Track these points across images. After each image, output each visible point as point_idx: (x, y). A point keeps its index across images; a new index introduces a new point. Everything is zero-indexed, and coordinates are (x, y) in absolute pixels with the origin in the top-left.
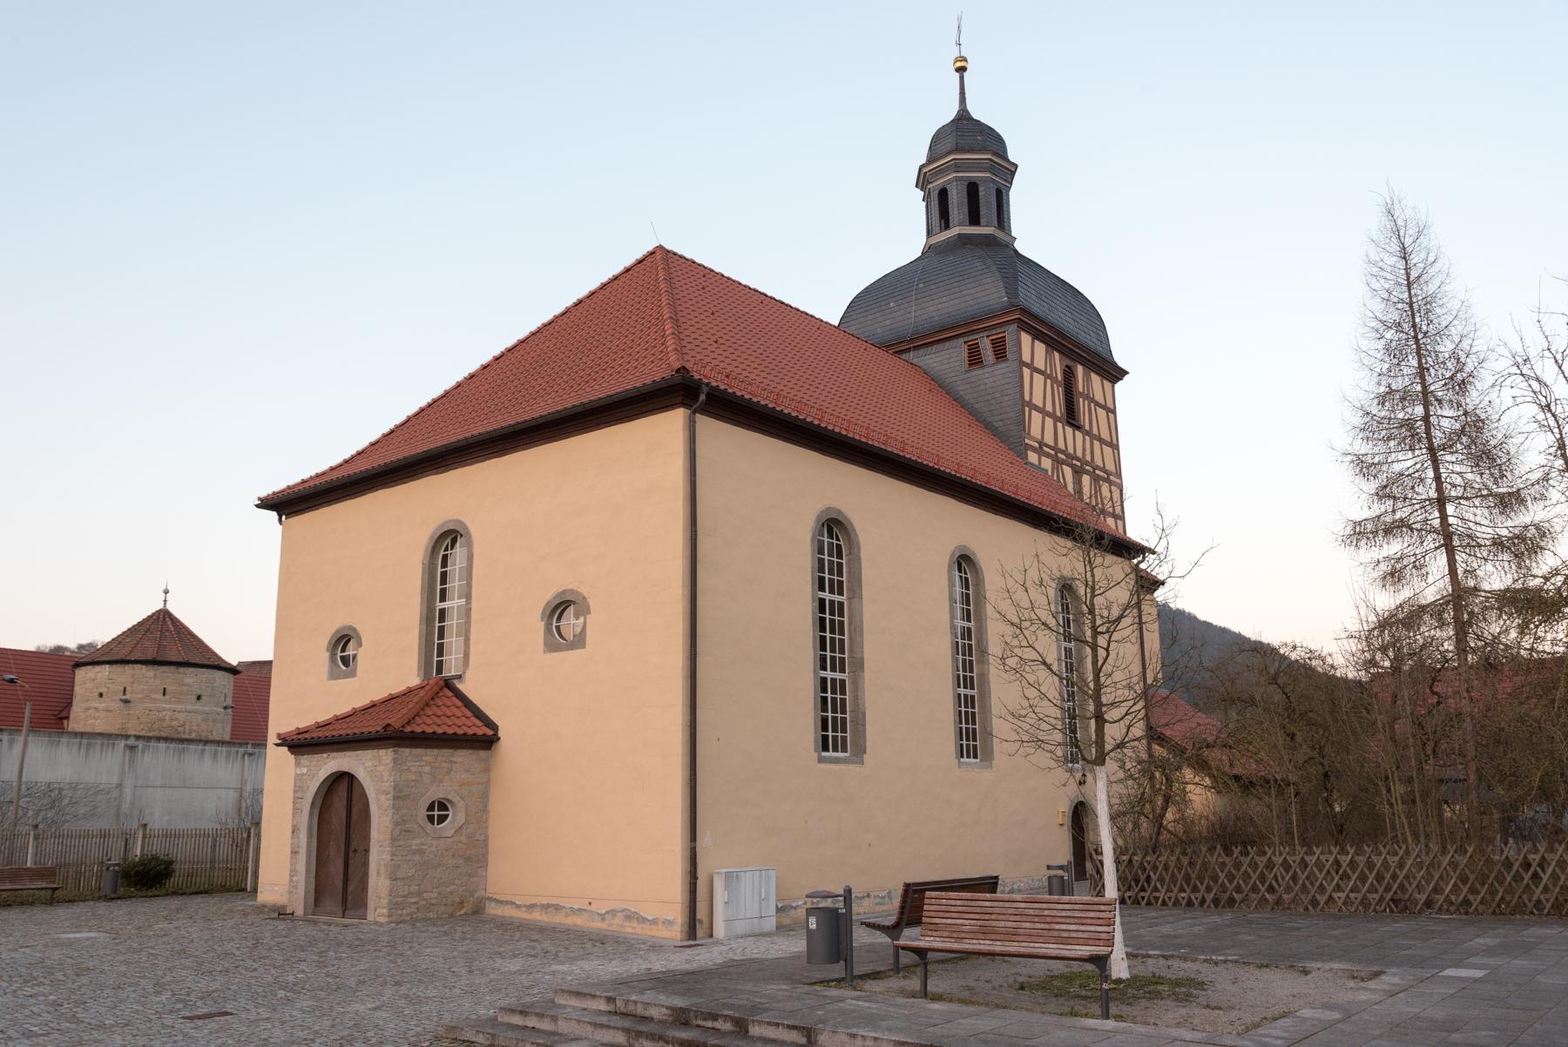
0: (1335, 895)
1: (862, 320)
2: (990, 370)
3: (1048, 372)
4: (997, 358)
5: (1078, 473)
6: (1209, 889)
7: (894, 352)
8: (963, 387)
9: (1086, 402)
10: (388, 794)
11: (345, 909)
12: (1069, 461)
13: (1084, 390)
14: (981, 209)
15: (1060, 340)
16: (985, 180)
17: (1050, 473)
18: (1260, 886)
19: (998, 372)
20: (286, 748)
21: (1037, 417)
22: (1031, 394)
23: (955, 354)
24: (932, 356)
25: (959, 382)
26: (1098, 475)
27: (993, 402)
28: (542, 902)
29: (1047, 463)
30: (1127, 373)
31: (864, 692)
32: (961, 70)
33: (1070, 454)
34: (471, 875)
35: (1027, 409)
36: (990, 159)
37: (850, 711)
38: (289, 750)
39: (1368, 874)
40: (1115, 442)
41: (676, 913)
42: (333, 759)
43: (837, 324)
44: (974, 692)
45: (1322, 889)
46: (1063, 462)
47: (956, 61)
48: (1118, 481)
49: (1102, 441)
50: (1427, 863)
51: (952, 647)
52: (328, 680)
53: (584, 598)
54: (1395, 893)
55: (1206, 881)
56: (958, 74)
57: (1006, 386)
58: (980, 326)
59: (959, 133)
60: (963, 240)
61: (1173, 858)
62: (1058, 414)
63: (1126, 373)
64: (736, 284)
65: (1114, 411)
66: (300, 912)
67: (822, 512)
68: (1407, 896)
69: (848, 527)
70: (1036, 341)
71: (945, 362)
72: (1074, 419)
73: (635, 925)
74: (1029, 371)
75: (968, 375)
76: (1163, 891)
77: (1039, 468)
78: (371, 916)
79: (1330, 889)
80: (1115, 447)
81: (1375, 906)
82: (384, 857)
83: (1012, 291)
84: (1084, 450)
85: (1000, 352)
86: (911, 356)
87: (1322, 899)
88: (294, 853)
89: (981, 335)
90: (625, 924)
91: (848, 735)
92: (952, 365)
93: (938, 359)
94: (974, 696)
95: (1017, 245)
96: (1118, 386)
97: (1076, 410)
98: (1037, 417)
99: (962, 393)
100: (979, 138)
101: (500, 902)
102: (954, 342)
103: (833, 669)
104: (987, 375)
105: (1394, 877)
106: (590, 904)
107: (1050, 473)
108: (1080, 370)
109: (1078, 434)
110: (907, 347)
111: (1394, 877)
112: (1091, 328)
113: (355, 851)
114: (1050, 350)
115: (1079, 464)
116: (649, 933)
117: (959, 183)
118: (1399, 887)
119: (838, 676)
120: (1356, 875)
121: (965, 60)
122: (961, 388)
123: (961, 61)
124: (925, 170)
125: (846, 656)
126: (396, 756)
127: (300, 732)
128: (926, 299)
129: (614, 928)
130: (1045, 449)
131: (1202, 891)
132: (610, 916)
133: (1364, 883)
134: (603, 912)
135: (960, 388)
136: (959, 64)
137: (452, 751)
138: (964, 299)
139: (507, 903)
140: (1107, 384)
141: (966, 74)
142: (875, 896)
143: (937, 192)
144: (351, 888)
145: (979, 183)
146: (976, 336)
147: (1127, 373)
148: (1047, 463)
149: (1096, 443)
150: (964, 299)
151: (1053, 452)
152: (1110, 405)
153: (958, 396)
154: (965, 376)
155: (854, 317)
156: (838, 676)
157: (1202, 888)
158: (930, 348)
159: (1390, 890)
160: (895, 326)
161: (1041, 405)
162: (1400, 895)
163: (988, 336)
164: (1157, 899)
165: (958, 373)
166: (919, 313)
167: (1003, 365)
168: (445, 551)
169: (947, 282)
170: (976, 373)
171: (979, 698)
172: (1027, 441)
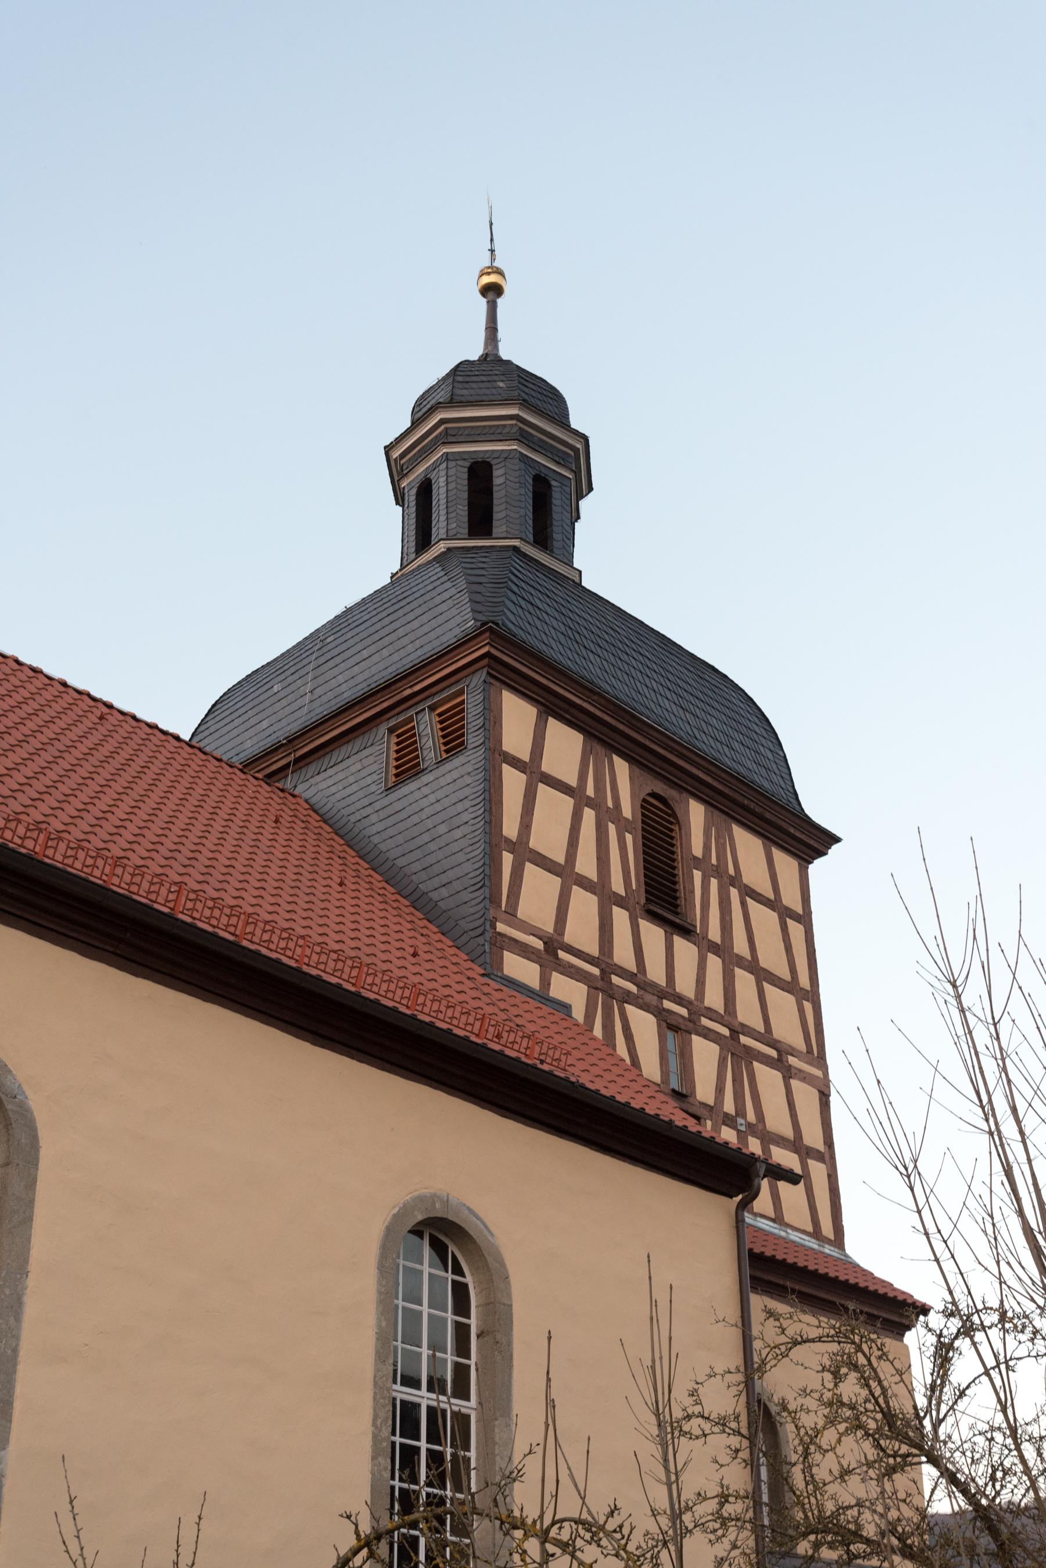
3: (590, 791)
4: (447, 751)
7: (269, 776)
8: (380, 827)
9: (714, 882)
12: (652, 999)
13: (707, 848)
14: (495, 509)
15: (621, 727)
16: (507, 456)
17: (579, 1014)
19: (449, 778)
23: (371, 759)
25: (374, 818)
27: (433, 846)
30: (837, 840)
33: (654, 985)
35: (507, 858)
40: (804, 981)
46: (627, 998)
48: (818, 1073)
49: (763, 976)
57: (460, 807)
58: (417, 688)
59: (460, 379)
62: (618, 886)
65: (805, 919)
70: (551, 721)
71: (352, 779)
72: (677, 914)
77: (542, 996)
92: (363, 783)
93: (341, 776)
95: (585, 583)
96: (817, 868)
97: (681, 894)
99: (376, 840)
100: (501, 384)
107: (579, 1014)
108: (696, 813)
109: (685, 950)
114: (600, 749)
117: (452, 464)
121: (500, 272)
123: (489, 274)
124: (395, 454)
130: (562, 954)
135: (374, 830)
136: (486, 280)
141: (500, 301)
143: (414, 491)
145: (493, 462)
147: (837, 840)
149: (744, 981)
151: (596, 971)
152: (791, 899)
154: (386, 801)
163: (432, 708)
165: (373, 798)
166: (319, 691)
167: (457, 761)
172: (501, 927)
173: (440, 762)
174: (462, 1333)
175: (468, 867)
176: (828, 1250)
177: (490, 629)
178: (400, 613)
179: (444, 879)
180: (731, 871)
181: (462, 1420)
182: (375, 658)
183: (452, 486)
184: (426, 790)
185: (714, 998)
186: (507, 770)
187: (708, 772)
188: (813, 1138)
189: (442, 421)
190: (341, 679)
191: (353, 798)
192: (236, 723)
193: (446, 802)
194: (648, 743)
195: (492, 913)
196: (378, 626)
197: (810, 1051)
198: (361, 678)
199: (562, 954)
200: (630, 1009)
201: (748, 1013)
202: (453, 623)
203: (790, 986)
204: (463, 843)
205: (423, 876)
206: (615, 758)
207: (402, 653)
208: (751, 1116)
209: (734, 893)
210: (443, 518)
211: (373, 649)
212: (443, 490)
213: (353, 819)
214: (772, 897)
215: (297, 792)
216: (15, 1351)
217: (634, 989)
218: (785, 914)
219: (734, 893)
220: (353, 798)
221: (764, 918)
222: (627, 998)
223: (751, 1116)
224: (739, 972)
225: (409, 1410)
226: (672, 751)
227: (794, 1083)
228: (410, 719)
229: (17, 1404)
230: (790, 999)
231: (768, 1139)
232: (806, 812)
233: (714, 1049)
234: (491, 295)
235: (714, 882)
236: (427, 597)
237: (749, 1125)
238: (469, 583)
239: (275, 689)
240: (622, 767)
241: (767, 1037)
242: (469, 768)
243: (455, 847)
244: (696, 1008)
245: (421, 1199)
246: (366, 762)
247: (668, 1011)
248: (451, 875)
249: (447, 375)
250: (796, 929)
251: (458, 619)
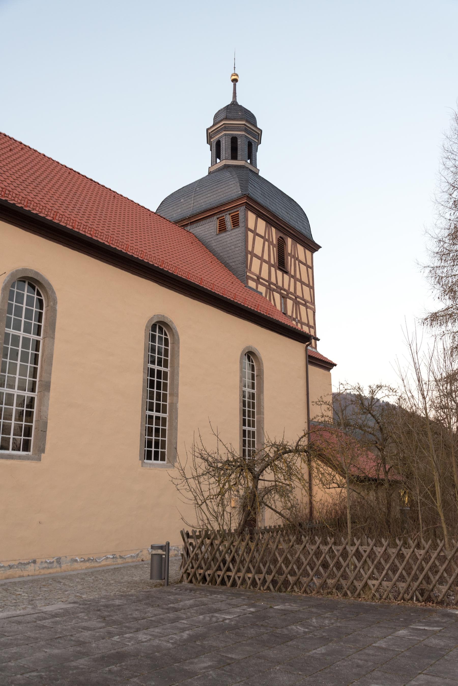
0: (370, 582)
1: (167, 210)
3: (267, 237)
4: (234, 226)
5: (284, 297)
6: (269, 572)
8: (215, 244)
9: (293, 259)
12: (279, 290)
13: (291, 251)
14: (238, 151)
15: (274, 220)
16: (242, 136)
17: (264, 295)
18: (310, 572)
19: (234, 234)
21: (255, 260)
22: (253, 247)
23: (212, 225)
25: (213, 241)
26: (299, 302)
27: (230, 251)
29: (262, 289)
30: (320, 247)
31: (48, 407)
33: (279, 287)
35: (249, 256)
36: (244, 124)
37: (36, 421)
39: (398, 565)
40: (311, 284)
43: (155, 212)
44: (255, 429)
45: (358, 577)
46: (274, 290)
47: (232, 75)
48: (313, 307)
49: (302, 283)
50: (449, 558)
51: (144, 382)
54: (421, 583)
55: (268, 564)
56: (233, 83)
57: (238, 242)
58: (225, 208)
60: (226, 167)
61: (244, 544)
62: (272, 262)
63: (320, 247)
64: (56, 164)
65: (312, 268)
67: (17, 271)
68: (431, 587)
69: (43, 282)
70: (259, 218)
71: (206, 230)
74: (252, 234)
75: (218, 237)
76: (234, 571)
77: (256, 291)
79: (366, 577)
80: (312, 287)
81: (403, 595)
83: (244, 187)
84: (289, 286)
85: (236, 224)
86: (188, 228)
87: (359, 585)
91: (32, 438)
92: (210, 232)
93: (203, 229)
94: (254, 432)
95: (259, 174)
96: (315, 254)
98: (255, 260)
99: (214, 247)
103: (249, 426)
105: (421, 569)
107: (264, 295)
108: (289, 241)
109: (286, 277)
110: (187, 223)
111: (421, 569)
112: (299, 219)
114: (269, 225)
115: (285, 293)
117: (226, 137)
118: (424, 578)
119: (251, 429)
120: (388, 565)
121: (237, 75)
122: (214, 244)
124: (210, 131)
125: (37, 380)
128: (199, 196)
130: (261, 280)
131: (264, 573)
133: (394, 572)
135: (213, 245)
136: (233, 77)
138: (219, 194)
141: (237, 84)
142: (42, 562)
143: (215, 143)
146: (223, 214)
147: (320, 247)
148: (262, 289)
149: (298, 284)
150: (219, 194)
151: (267, 284)
152: (309, 263)
153: (212, 249)
155: (163, 209)
156: (251, 429)
157: (264, 570)
158: (199, 223)
159: (417, 579)
160: (183, 212)
161: (260, 255)
162: (424, 586)
163: (229, 214)
164: (229, 577)
165: (213, 236)
166: (195, 204)
167: (237, 230)
169: (211, 186)
171: (170, 419)
172: (248, 274)
173: (232, 229)
174: (253, 376)
175: (240, 258)
176: (314, 350)
177: (247, 196)
178: (219, 185)
179: (233, 260)
180: (297, 256)
181: (166, 373)
182: (212, 197)
183: (227, 143)
184: (228, 236)
185: (292, 290)
186: (249, 233)
187: (293, 231)
188: (311, 323)
189: (224, 124)
190: (202, 201)
191: (207, 235)
192: (170, 209)
193: (234, 240)
194: (280, 224)
195: (246, 271)
196: (212, 188)
197: (312, 302)
198: (208, 202)
199: (261, 280)
200: (274, 293)
201: (299, 293)
202: (235, 191)
203: (308, 286)
204: (239, 252)
205: (227, 259)
206: (272, 228)
207: (220, 197)
208: (299, 318)
209: (297, 262)
210: (224, 153)
211: (211, 194)
212: (224, 144)
213: (207, 241)
214: (305, 262)
215: (190, 231)
216: (178, 383)
217: (275, 288)
218: (308, 267)
219: (297, 262)
220: (207, 235)
221: (303, 268)
222: (274, 290)
223: (299, 318)
224: (267, 260)
225: (152, 371)
226: (287, 227)
227: (308, 310)
228: (223, 216)
229: (179, 394)
230: (308, 288)
231: (302, 324)
232: (314, 239)
233: (292, 302)
234: (235, 82)
235: (293, 259)
236: (227, 182)
237: (298, 320)
238: (239, 180)
239: (182, 201)
240: (274, 230)
241: (303, 299)
242: (240, 232)
243: (236, 252)
244: (288, 292)
245: (247, 347)
246: (210, 226)
247: (283, 293)
248: (235, 259)
249: (224, 108)
250: (310, 270)
251: (236, 190)
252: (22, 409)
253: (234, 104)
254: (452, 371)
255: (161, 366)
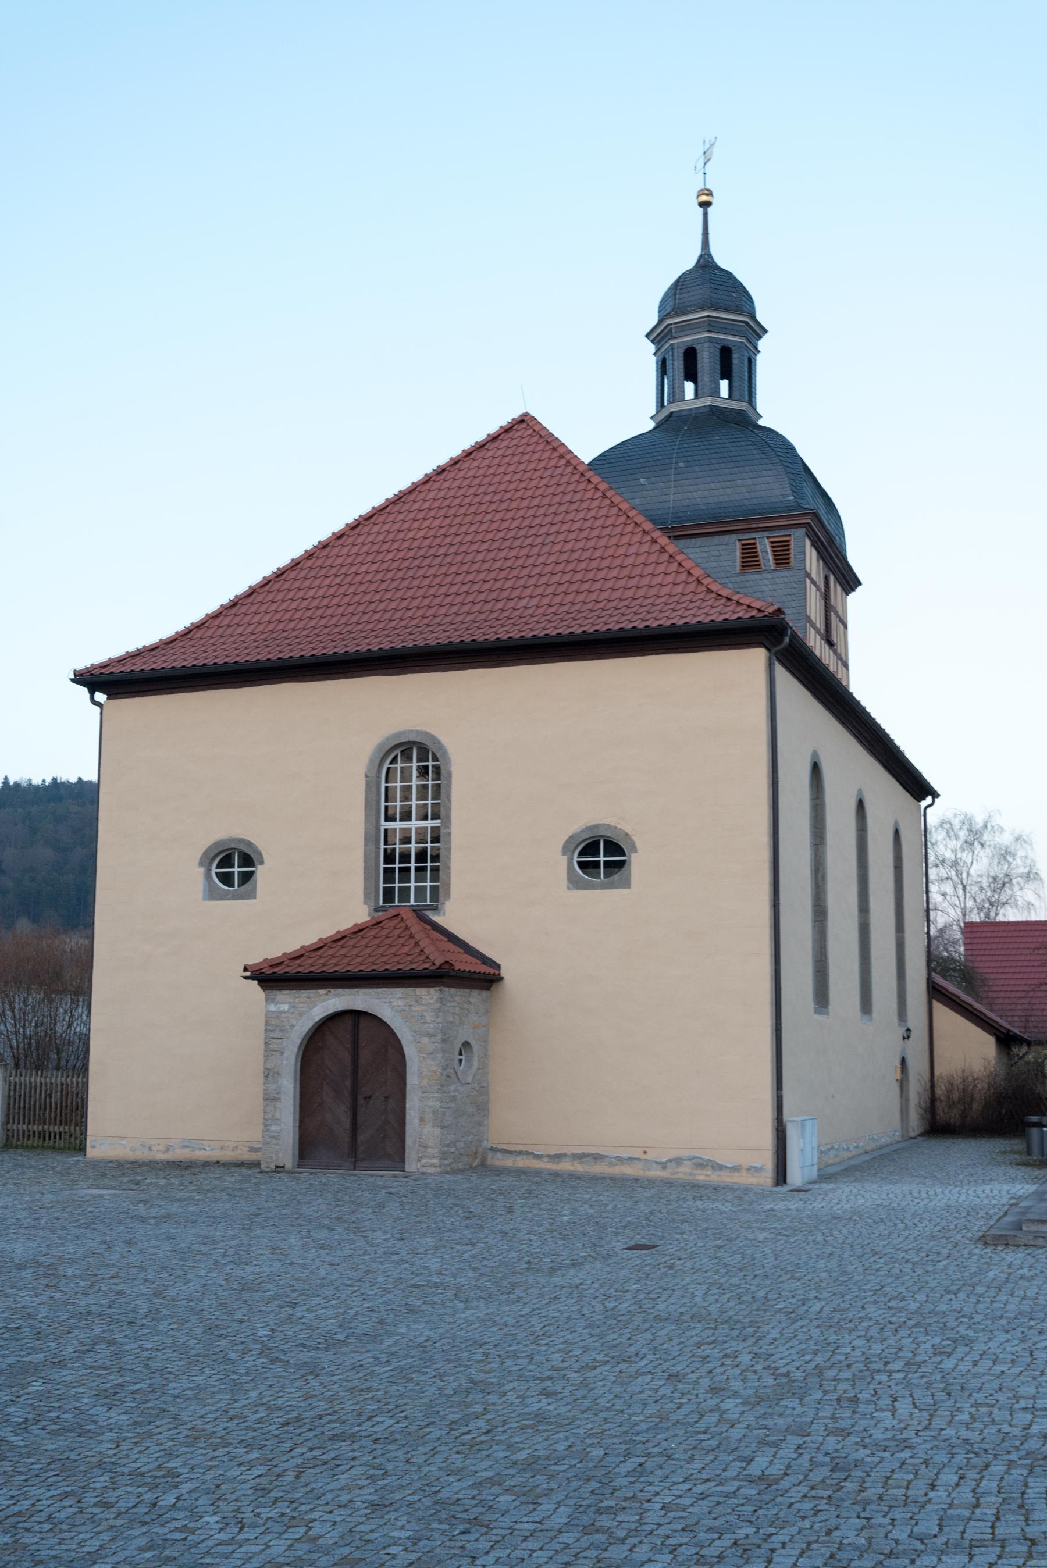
2: (769, 576)
10: (434, 1036)
11: (356, 1161)
16: (740, 346)
20: (256, 982)
24: (697, 550)
28: (575, 1152)
32: (705, 205)
34: (480, 1124)
36: (746, 323)
38: (259, 984)
41: (767, 1161)
42: (336, 996)
47: (701, 193)
52: (204, 899)
53: (627, 835)
56: (701, 210)
58: (761, 525)
66: (289, 1165)
73: (709, 1173)
78: (412, 1165)
82: (430, 1103)
85: (782, 556)
88: (270, 1099)
89: (760, 534)
90: (695, 1172)
93: (705, 555)
100: (734, 295)
101: (510, 1152)
102: (726, 538)
104: (767, 582)
106: (645, 1152)
113: (368, 1098)
116: (728, 1180)
121: (710, 193)
126: (442, 996)
127: (277, 963)
129: (680, 1176)
132: (673, 1164)
134: (664, 1160)
136: (704, 198)
137: (468, 991)
139: (520, 1153)
140: (844, 594)
141: (710, 210)
143: (682, 351)
144: (361, 1138)
145: (733, 348)
146: (753, 535)
154: (738, 579)
167: (786, 573)
168: (391, 763)
170: (751, 577)
226: (837, 556)
252: (429, 840)
253: (706, 264)
254: (957, 1201)
255: (217, 868)
